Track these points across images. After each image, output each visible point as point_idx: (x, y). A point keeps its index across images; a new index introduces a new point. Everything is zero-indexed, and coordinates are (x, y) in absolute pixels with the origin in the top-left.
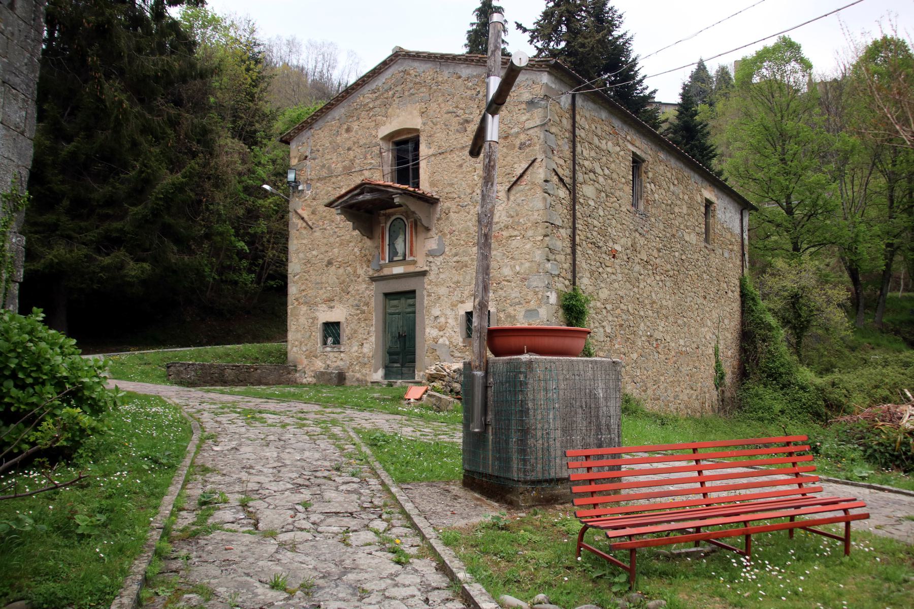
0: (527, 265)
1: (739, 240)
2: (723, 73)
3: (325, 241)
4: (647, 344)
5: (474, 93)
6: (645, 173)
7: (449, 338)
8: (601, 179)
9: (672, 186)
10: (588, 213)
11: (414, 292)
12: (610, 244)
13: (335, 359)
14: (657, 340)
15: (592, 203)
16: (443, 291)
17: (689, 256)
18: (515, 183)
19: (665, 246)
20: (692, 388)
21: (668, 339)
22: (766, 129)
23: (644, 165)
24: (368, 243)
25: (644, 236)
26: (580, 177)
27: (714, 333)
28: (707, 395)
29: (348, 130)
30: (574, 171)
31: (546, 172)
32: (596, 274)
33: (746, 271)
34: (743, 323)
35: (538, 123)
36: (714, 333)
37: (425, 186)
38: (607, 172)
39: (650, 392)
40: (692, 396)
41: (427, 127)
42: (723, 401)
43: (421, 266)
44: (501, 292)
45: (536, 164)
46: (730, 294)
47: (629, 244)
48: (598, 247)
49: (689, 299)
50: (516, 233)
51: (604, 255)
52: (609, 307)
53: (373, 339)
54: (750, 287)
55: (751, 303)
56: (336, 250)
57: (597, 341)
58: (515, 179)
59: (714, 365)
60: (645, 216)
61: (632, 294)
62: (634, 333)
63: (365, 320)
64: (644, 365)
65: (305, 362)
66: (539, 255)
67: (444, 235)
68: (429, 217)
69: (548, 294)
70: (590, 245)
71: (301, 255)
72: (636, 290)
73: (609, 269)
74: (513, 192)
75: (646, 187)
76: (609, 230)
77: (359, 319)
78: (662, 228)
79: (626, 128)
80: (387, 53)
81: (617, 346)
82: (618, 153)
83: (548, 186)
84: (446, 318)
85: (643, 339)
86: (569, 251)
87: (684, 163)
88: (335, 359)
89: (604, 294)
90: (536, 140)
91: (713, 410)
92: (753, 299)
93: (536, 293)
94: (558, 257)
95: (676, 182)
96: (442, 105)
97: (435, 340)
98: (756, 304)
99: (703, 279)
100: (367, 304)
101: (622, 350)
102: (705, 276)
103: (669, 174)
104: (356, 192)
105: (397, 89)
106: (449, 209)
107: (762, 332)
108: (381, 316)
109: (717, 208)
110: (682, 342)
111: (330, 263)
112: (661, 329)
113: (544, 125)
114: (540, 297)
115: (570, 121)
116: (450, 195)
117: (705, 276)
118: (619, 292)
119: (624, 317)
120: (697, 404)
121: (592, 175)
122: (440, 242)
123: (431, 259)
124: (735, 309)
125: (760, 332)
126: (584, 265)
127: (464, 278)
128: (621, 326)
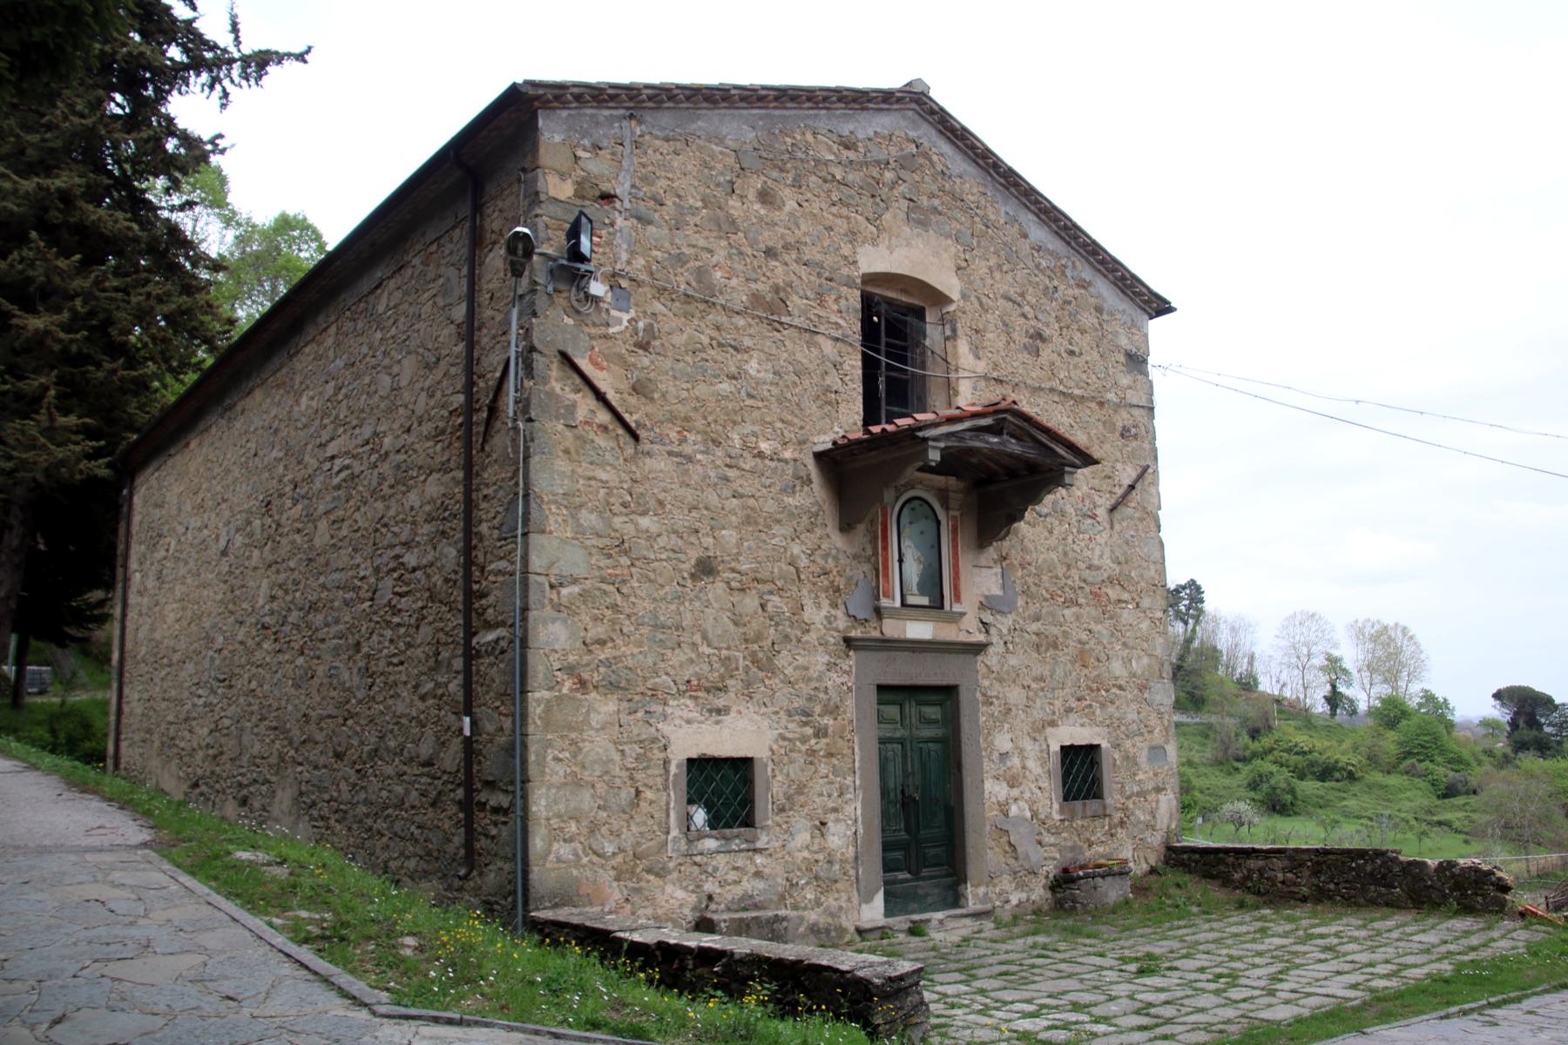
0: (1145, 660)
63: (830, 755)
74: (1117, 515)
80: (892, 80)
97: (1004, 808)
100: (833, 710)
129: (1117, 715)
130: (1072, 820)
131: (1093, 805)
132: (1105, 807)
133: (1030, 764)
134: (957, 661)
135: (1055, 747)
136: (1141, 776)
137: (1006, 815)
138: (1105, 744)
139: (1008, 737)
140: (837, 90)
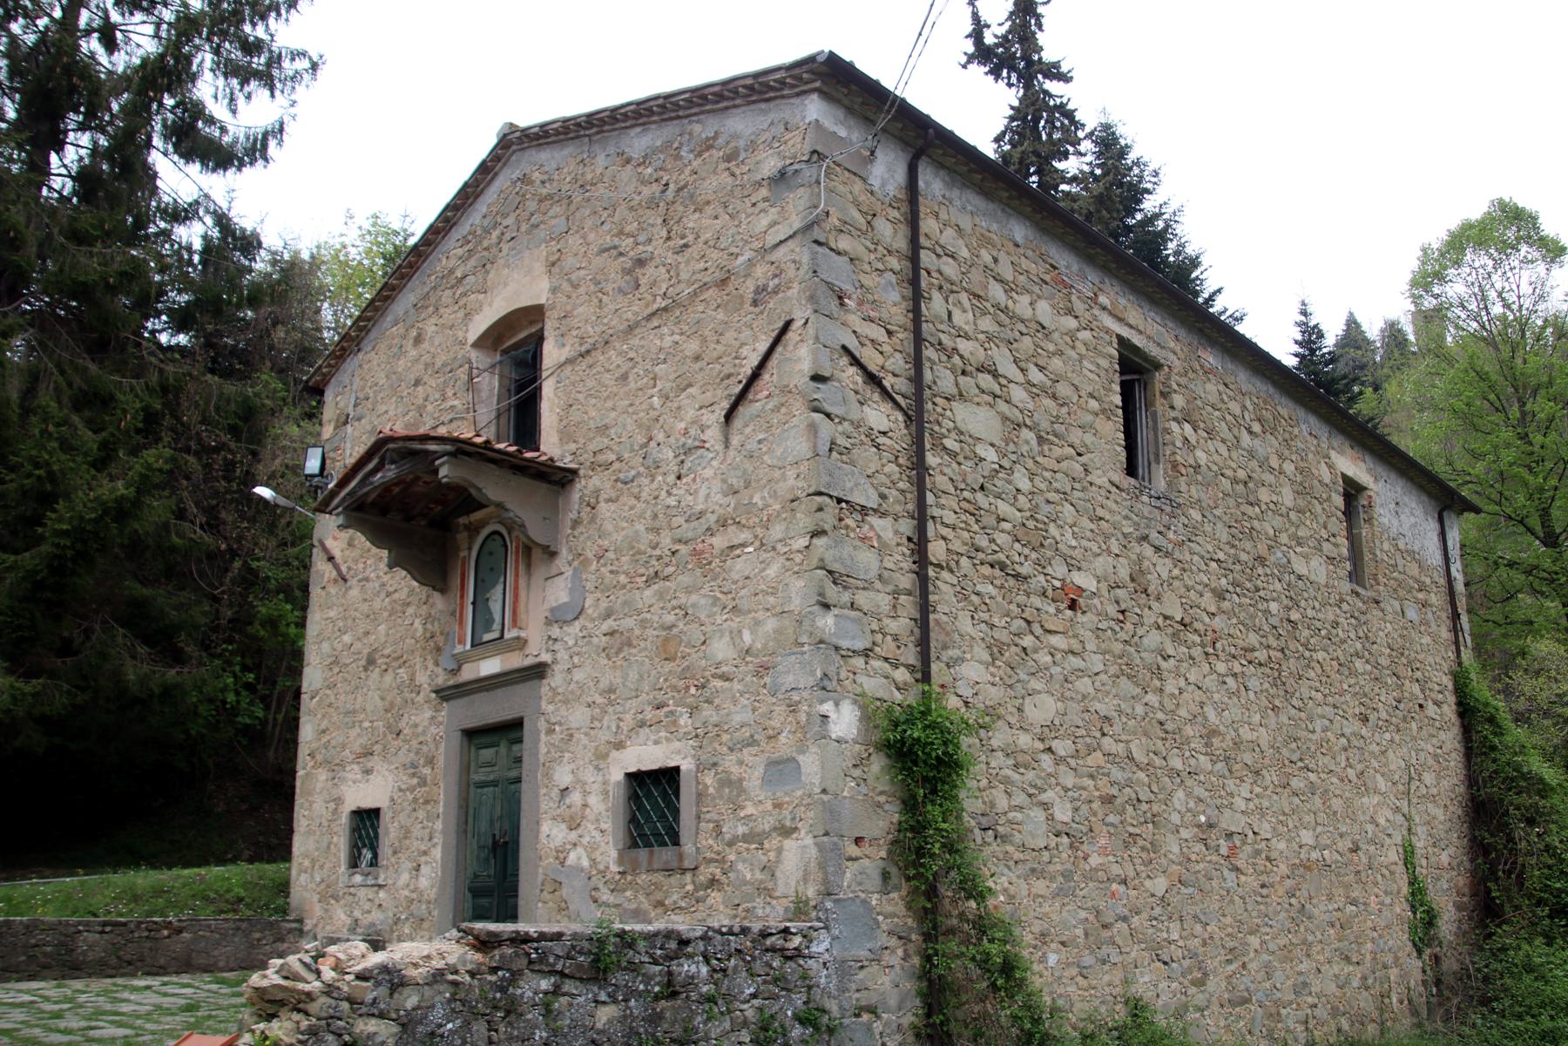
0: (771, 624)
1: (1442, 581)
2: (1393, 332)
3: (365, 607)
4: (1199, 847)
5: (656, 188)
6: (1164, 395)
7: (592, 848)
8: (1018, 394)
9: (1246, 439)
10: (975, 479)
11: (517, 724)
12: (1059, 569)
13: (367, 906)
14: (1230, 835)
15: (991, 455)
16: (578, 716)
17: (1310, 613)
18: (741, 398)
19: (1235, 584)
20: (1347, 959)
21: (1265, 830)
22: (1482, 376)
23: (1159, 377)
24: (437, 598)
25: (1168, 554)
26: (941, 377)
27: (1397, 809)
28: (1394, 973)
29: (418, 340)
30: (918, 362)
31: (814, 353)
32: (1011, 653)
33: (1467, 656)
34: (1472, 780)
35: (797, 225)
36: (1397, 809)
37: (551, 445)
38: (1036, 376)
39: (1215, 985)
40: (1347, 982)
41: (561, 298)
42: (1438, 982)
43: (536, 652)
44: (708, 712)
45: (791, 336)
46: (1431, 709)
47: (1124, 573)
48: (1017, 576)
49: (1318, 724)
50: (745, 536)
51: (1036, 601)
52: (1062, 747)
53: (437, 853)
54: (1481, 689)
55: (1486, 729)
56: (382, 628)
57: (1023, 847)
58: (738, 389)
59: (1405, 890)
60: (1169, 503)
61: (1140, 710)
62: (1154, 820)
63: (427, 802)
64: (1191, 909)
65: (318, 910)
66: (798, 592)
67: (585, 563)
68: (552, 516)
69: (827, 708)
70: (986, 570)
71: (326, 646)
72: (1152, 698)
73: (1055, 640)
74: (737, 423)
75: (1168, 431)
76: (1053, 530)
77: (415, 800)
78: (1225, 537)
79: (1093, 276)
80: (482, 146)
81: (1095, 860)
82: (1072, 334)
83: (823, 393)
84: (586, 793)
85: (1184, 834)
86: (906, 581)
87: (1275, 384)
88: (367, 906)
89: (1043, 709)
90: (791, 272)
91: (1415, 1012)
92: (1492, 720)
93: (793, 708)
94: (862, 599)
95: (1256, 428)
96: (591, 237)
97: (561, 855)
98: (1499, 731)
99: (1353, 673)
100: (430, 761)
101: (1116, 870)
102: (1359, 665)
103: (1235, 408)
104: (371, 466)
105: (505, 223)
106: (597, 492)
107: (1524, 799)
108: (454, 789)
109: (1377, 500)
110: (1307, 837)
111: (371, 661)
112: (1240, 804)
113: (808, 227)
114: (803, 718)
115: (904, 230)
116: (601, 458)
117: (1359, 665)
118: (1098, 706)
119: (1117, 774)
120: (1365, 1002)
121: (986, 380)
122: (578, 589)
123: (555, 631)
124: (1448, 746)
125: (1517, 800)
126: (965, 624)
127: (625, 677)
128: (1108, 800)
129: (715, 719)
130: (634, 871)
131: (665, 855)
132: (681, 857)
133: (593, 800)
134: (521, 690)
135: (617, 776)
136: (750, 809)
137: (562, 864)
138: (686, 766)
139: (568, 768)
140: (447, 208)
